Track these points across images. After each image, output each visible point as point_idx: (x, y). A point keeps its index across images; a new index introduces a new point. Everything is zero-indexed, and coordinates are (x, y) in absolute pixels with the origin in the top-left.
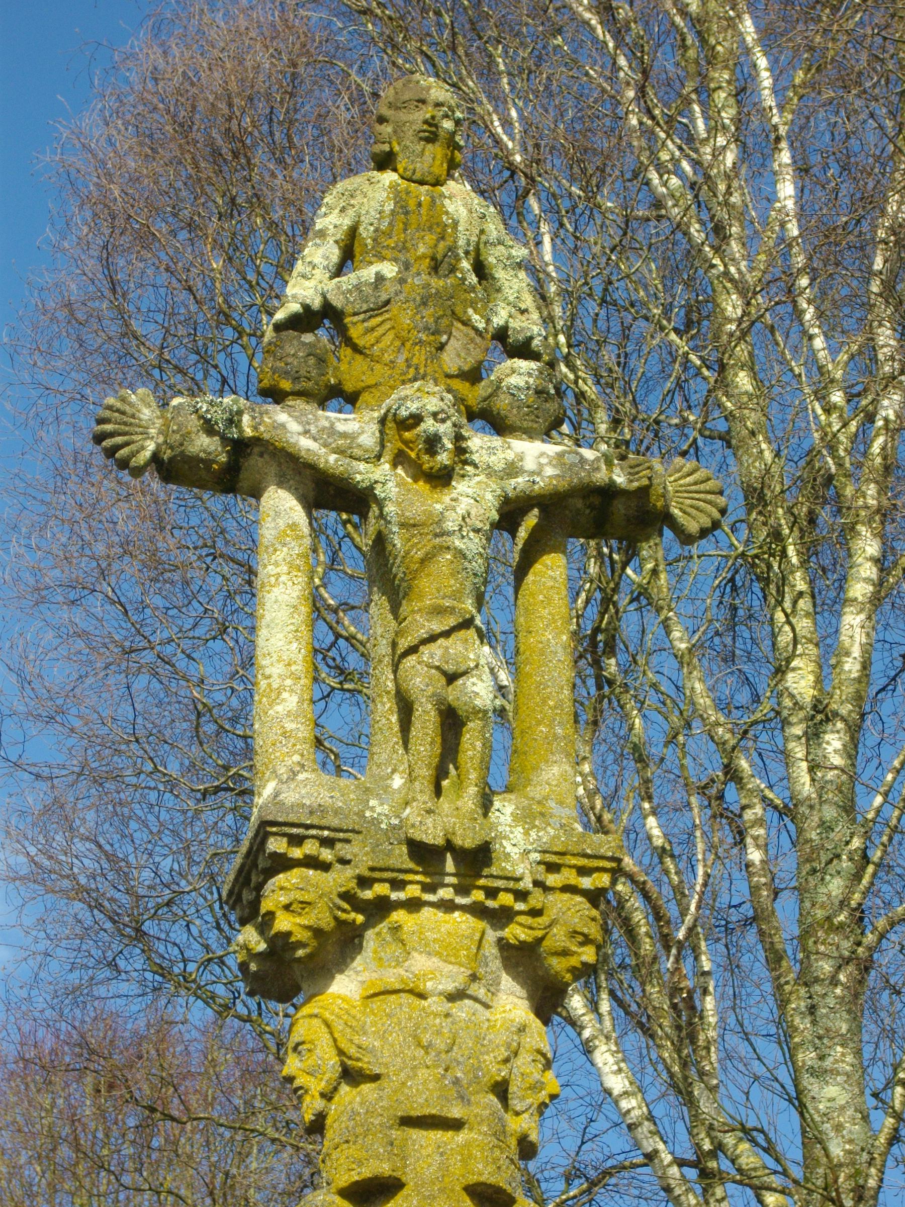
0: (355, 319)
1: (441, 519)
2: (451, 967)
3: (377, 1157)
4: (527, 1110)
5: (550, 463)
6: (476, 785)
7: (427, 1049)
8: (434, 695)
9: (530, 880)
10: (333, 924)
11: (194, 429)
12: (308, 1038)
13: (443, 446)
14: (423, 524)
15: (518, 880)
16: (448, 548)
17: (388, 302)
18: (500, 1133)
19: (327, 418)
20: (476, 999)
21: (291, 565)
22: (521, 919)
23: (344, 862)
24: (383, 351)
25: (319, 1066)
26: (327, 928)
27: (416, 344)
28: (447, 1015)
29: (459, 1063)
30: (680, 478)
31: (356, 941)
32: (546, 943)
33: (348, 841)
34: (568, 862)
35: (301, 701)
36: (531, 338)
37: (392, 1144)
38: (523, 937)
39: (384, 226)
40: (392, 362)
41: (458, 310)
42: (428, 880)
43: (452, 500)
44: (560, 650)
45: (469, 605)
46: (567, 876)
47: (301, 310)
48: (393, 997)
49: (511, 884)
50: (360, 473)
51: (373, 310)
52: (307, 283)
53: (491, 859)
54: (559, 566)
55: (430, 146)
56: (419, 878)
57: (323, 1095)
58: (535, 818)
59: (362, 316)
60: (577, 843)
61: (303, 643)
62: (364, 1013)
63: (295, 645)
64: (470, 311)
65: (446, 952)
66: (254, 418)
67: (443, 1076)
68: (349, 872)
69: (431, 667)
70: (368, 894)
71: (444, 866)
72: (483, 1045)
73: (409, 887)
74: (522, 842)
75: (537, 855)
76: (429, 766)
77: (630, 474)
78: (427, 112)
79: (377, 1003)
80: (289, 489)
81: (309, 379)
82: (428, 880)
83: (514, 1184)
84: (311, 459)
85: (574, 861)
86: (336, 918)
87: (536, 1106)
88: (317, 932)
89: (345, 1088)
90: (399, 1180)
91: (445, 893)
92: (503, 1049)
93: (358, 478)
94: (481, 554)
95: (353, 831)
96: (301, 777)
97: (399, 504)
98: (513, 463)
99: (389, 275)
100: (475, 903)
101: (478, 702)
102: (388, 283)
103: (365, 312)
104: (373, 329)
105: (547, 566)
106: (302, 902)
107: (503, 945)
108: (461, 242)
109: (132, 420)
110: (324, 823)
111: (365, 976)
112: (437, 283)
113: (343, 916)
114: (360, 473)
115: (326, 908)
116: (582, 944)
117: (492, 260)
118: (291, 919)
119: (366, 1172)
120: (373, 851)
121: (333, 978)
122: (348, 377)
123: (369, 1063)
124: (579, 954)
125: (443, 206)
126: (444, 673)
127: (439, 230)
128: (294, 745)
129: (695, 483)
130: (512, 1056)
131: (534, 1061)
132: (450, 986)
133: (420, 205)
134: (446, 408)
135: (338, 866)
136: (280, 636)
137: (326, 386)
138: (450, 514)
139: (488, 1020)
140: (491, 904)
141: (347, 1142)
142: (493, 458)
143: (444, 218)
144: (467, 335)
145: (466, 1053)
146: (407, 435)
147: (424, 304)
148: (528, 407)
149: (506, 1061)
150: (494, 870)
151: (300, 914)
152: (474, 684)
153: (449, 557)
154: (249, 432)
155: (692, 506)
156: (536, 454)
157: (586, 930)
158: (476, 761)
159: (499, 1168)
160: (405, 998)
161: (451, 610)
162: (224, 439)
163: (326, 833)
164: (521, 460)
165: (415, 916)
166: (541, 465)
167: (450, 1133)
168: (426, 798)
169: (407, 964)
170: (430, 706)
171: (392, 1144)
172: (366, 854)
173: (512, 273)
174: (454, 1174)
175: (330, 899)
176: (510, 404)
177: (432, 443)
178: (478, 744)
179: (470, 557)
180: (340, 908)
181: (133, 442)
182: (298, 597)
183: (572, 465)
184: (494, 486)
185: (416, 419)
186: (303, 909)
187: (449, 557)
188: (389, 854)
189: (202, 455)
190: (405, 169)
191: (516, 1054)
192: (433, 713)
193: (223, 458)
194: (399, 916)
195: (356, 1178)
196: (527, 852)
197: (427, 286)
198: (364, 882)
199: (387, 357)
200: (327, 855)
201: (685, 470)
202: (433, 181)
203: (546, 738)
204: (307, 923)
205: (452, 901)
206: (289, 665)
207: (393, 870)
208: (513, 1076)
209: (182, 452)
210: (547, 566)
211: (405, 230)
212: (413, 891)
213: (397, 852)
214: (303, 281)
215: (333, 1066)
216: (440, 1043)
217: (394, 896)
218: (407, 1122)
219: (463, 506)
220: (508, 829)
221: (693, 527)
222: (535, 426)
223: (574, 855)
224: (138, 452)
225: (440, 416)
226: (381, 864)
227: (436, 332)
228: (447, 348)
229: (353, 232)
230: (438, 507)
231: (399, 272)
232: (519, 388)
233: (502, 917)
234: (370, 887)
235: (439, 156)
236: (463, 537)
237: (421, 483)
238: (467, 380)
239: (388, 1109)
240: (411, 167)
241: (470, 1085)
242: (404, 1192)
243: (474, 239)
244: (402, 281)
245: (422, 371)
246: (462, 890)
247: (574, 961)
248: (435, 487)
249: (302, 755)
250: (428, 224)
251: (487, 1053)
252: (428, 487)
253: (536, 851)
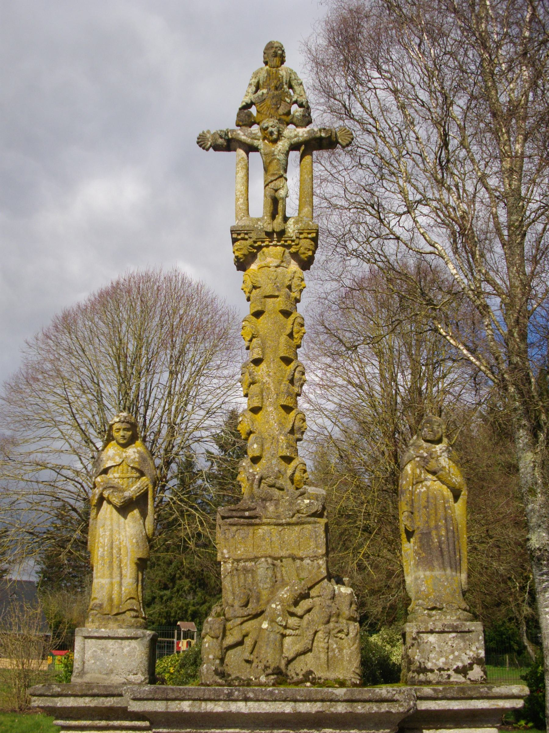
7: (270, 279)
18: (288, 297)
23: (250, 238)
45: (282, 172)
65: (275, 256)
68: (252, 240)
70: (256, 245)
78: (274, 50)
79: (260, 270)
88: (244, 255)
89: (254, 290)
91: (274, 243)
107: (290, 253)
108: (284, 81)
112: (277, 93)
119: (256, 310)
132: (276, 264)
154: (230, 137)
160: (266, 268)
161: (276, 174)
162: (225, 139)
177: (271, 133)
185: (267, 128)
194: (264, 249)
198: (255, 242)
200: (246, 237)
212: (267, 243)
221: (344, 144)
227: (277, 105)
229: (258, 83)
233: (289, 247)
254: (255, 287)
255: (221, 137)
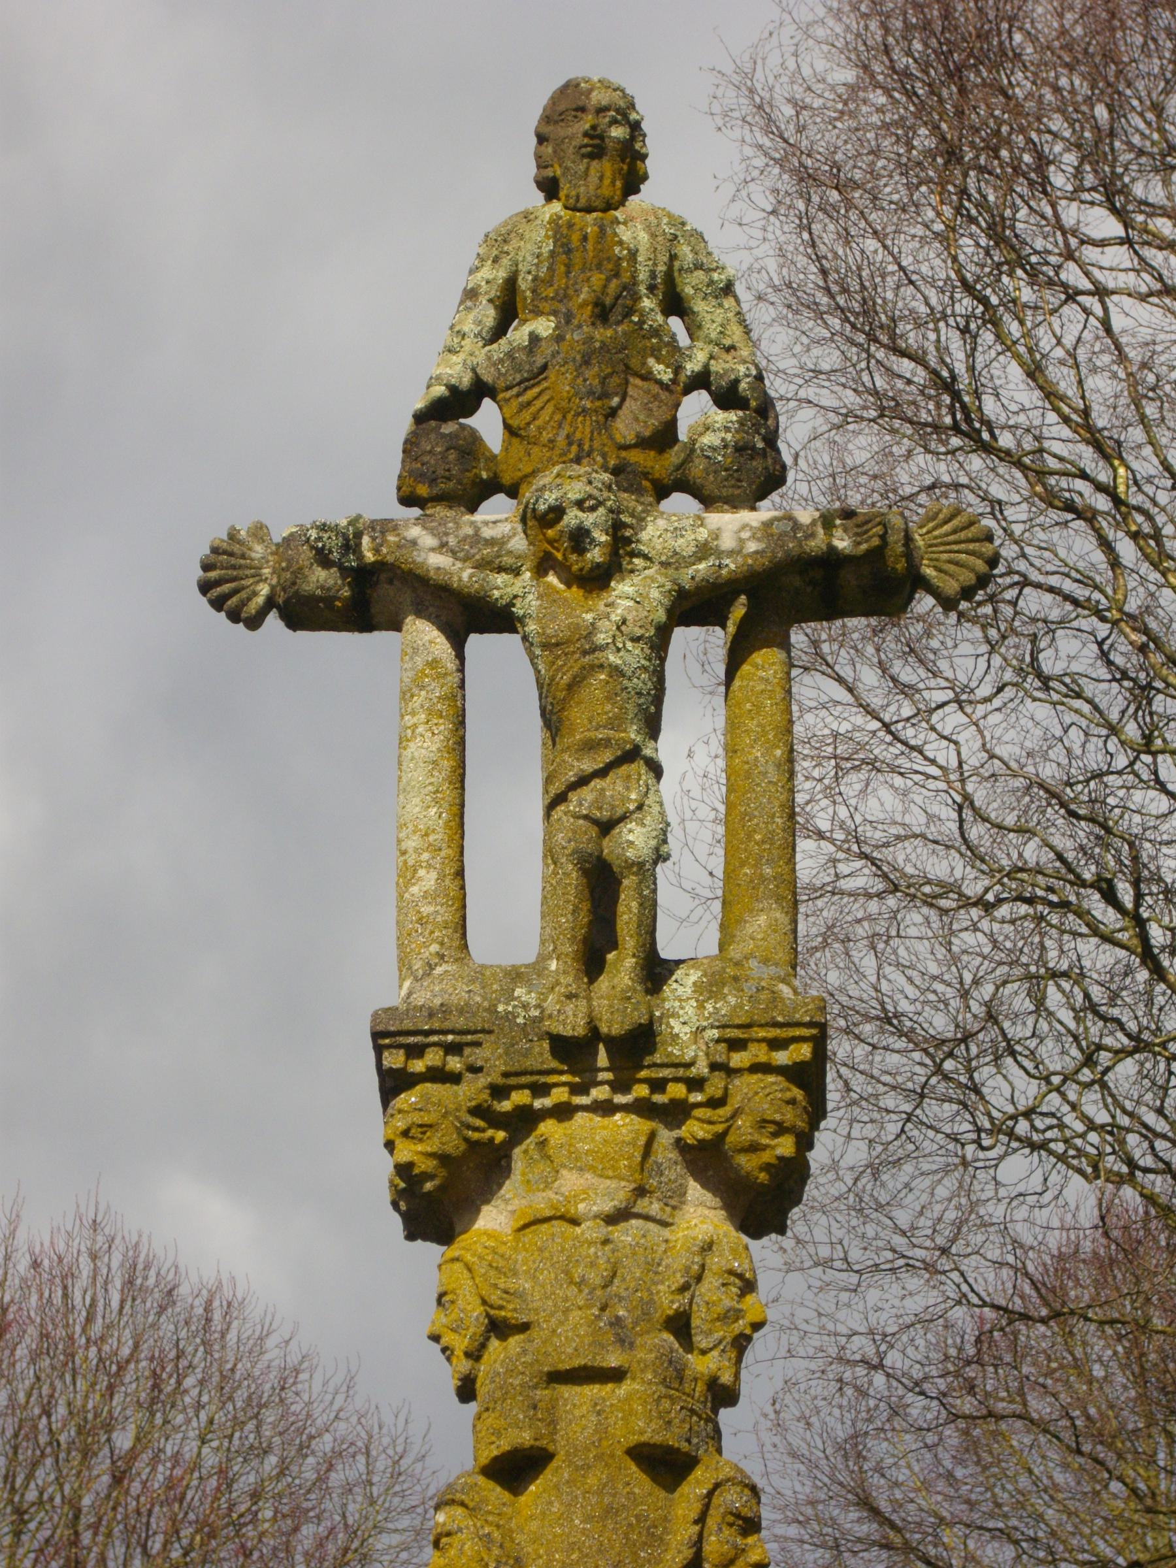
0: (508, 394)
1: (593, 628)
2: (608, 1182)
3: (517, 1425)
4: (715, 1347)
5: (753, 537)
6: (634, 956)
7: (581, 1284)
8: (575, 852)
9: (705, 1063)
10: (463, 1147)
11: (307, 563)
12: (450, 1287)
13: (593, 540)
14: (568, 642)
15: (688, 1065)
16: (601, 666)
17: (544, 368)
18: (676, 1376)
19: (472, 523)
20: (647, 1218)
21: (430, 712)
22: (698, 1113)
23: (475, 1070)
24: (540, 429)
25: (461, 1320)
26: (455, 1153)
27: (579, 414)
28: (606, 1242)
29: (621, 1299)
30: (935, 528)
31: (503, 1163)
32: (730, 1139)
33: (478, 1044)
34: (754, 1035)
35: (441, 878)
36: (737, 381)
37: (535, 1407)
38: (701, 1134)
39: (543, 272)
40: (551, 441)
41: (634, 363)
42: (577, 1079)
43: (607, 605)
44: (771, 769)
45: (633, 734)
46: (758, 1053)
47: (447, 393)
48: (545, 1226)
49: (681, 1072)
50: (498, 588)
51: (528, 380)
52: (454, 358)
53: (655, 1044)
54: (773, 664)
55: (595, 163)
56: (564, 1078)
57: (468, 1355)
58: (724, 985)
59: (515, 390)
60: (765, 1010)
61: (446, 805)
62: (515, 1249)
63: (433, 811)
64: (651, 361)
65: (601, 1165)
66: (374, 539)
67: (598, 1318)
69: (579, 817)
70: (506, 1106)
71: (596, 1060)
72: (656, 1273)
73: (555, 1091)
74: (694, 1019)
75: (715, 1031)
76: (573, 939)
77: (857, 534)
80: (429, 619)
81: (449, 479)
82: (577, 1079)
83: (695, 1441)
84: (441, 578)
85: (762, 1034)
86: (466, 1140)
87: (729, 1339)
88: (443, 1159)
89: (494, 1343)
90: (544, 1450)
91: (599, 1093)
92: (678, 1275)
93: (496, 593)
94: (645, 668)
95: (483, 1031)
96: (439, 970)
97: (539, 620)
98: (706, 543)
99: (544, 334)
100: (637, 1100)
101: (630, 854)
102: (543, 343)
103: (519, 384)
104: (529, 404)
105: (756, 666)
106: (421, 1126)
107: (679, 1143)
108: (643, 276)
109: (242, 562)
110: (447, 1025)
111: (516, 1204)
112: (603, 334)
113: (476, 1136)
114: (498, 588)
115: (452, 1130)
116: (775, 1135)
117: (689, 291)
118: (413, 1147)
119: (505, 1445)
120: (507, 1053)
121: (478, 1211)
122: (504, 467)
123: (515, 1310)
124: (773, 1148)
125: (616, 234)
126: (596, 822)
127: (610, 266)
128: (432, 932)
129: (954, 532)
130: (692, 1282)
131: (724, 1285)
132: (607, 1206)
133: (585, 238)
134: (596, 493)
135: (469, 1075)
136: (416, 801)
137: (474, 483)
138: (604, 624)
139: (667, 1241)
140: (658, 1098)
141: (487, 1409)
142: (681, 541)
143: (617, 250)
144: (648, 392)
145: (632, 1285)
146: (550, 533)
147: (586, 362)
148: (726, 470)
149: (684, 1288)
150: (658, 1058)
151: (421, 1140)
152: (630, 831)
153: (603, 677)
154: (370, 556)
155: (950, 562)
156: (736, 527)
157: (778, 1117)
158: (633, 926)
159: (669, 1423)
161: (606, 743)
162: (344, 571)
163: (450, 1037)
164: (717, 538)
165: (566, 1124)
166: (742, 541)
167: (610, 1386)
168: (570, 979)
169: (556, 1184)
170: (570, 867)
171: (535, 1407)
172: (500, 1057)
173: (714, 302)
174: (614, 1435)
175: (457, 1118)
176: (706, 469)
177: (579, 538)
178: (634, 904)
179: (629, 673)
180: (469, 1127)
181: (243, 588)
182: (439, 750)
183: (782, 535)
184: (661, 579)
185: (557, 512)
186: (424, 1133)
187: (603, 677)
188: (526, 1054)
189: (318, 592)
190: (567, 196)
191: (699, 1279)
192: (574, 875)
193: (346, 593)
194: (547, 1127)
195: (495, 1453)
196: (700, 1030)
197: (591, 339)
198: (499, 1092)
199: (546, 437)
200: (455, 1064)
201: (941, 516)
202: (602, 206)
203: (752, 881)
204: (429, 1149)
205: (609, 1101)
206: (427, 835)
207: (532, 1073)
208: (695, 1307)
209: (297, 592)
210: (756, 666)
211: (568, 272)
212: (560, 1095)
213: (537, 1050)
214: (450, 356)
215: (477, 1319)
216: (594, 1277)
217: (538, 1104)
218: (558, 1377)
219: (619, 611)
220: (677, 1004)
222: (737, 492)
223: (761, 1026)
224: (249, 599)
225: (587, 504)
226: (516, 1067)
227: (605, 395)
228: (620, 413)
229: (511, 284)
230: (589, 617)
231: (557, 328)
232: (714, 449)
233: (676, 1113)
234: (508, 1097)
235: (608, 174)
236: (619, 650)
237: (574, 589)
238: (651, 448)
239: (532, 1364)
240: (573, 193)
241: (636, 1324)
242: (554, 1464)
243: (661, 268)
244: (559, 338)
245: (586, 447)
246: (620, 1086)
247: (766, 1157)
248: (591, 592)
249: (442, 944)
250: (595, 261)
251: (662, 1282)
252: (581, 592)
253: (712, 1027)
254: (498, 1328)
255: (323, 558)
